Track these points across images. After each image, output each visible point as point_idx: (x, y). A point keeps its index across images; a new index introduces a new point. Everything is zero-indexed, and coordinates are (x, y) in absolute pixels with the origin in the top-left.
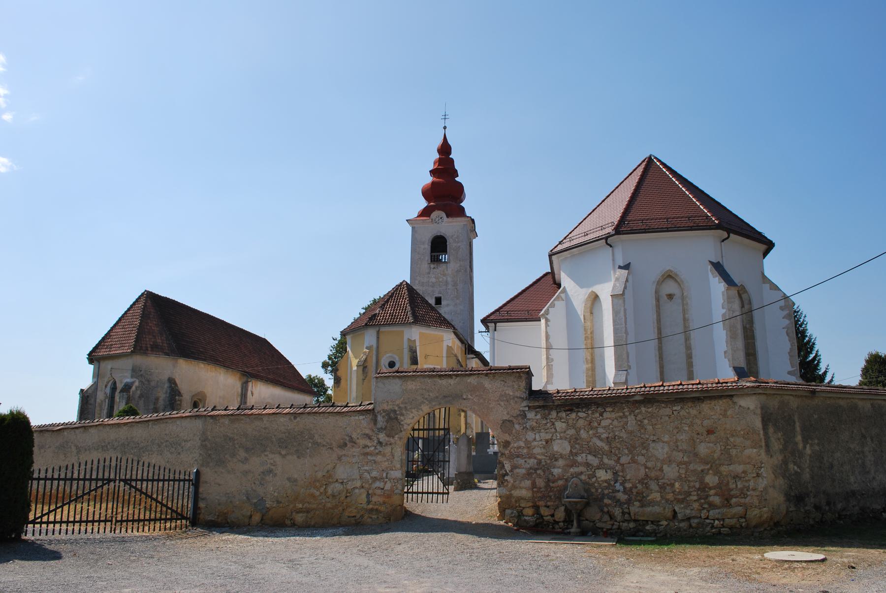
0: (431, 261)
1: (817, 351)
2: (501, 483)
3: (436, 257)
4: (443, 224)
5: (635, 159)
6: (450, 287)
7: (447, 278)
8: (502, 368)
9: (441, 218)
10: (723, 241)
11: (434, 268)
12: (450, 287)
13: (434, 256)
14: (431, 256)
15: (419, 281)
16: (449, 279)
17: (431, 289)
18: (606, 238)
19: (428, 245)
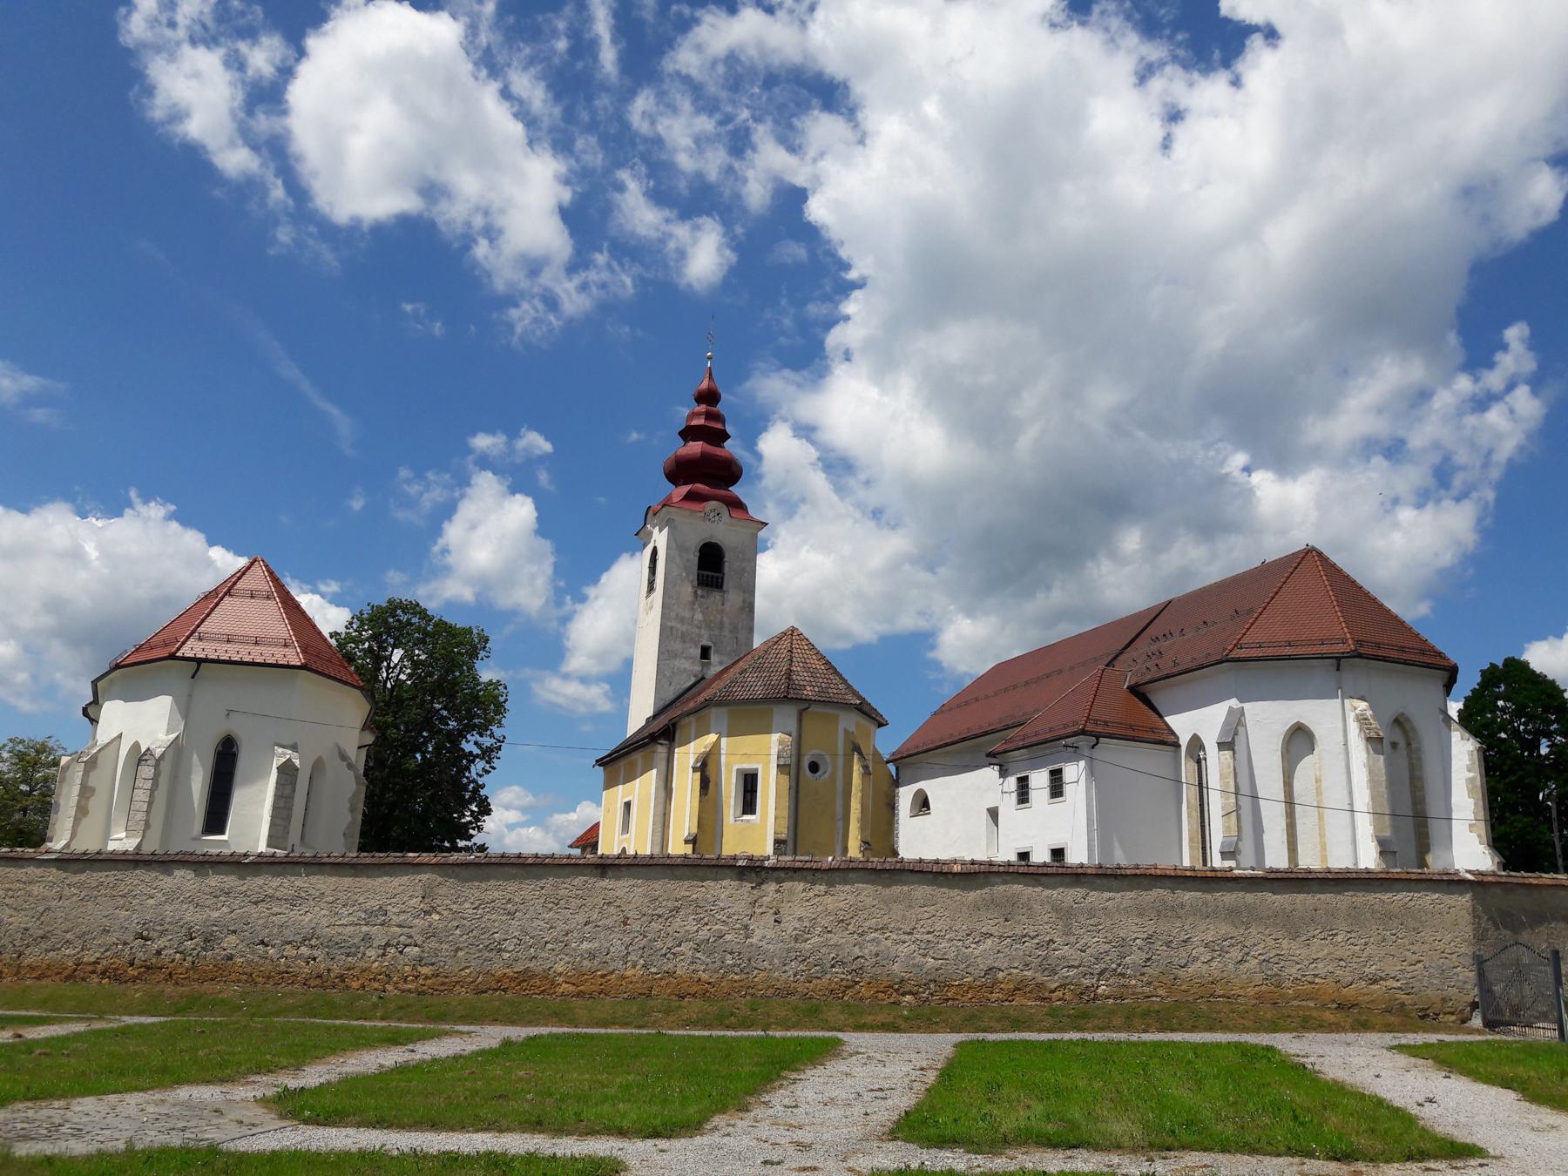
0: (698, 584)
1: (655, 541)
2: (595, 1021)
3: (715, 580)
4: (721, 524)
5: (985, 811)
6: (726, 633)
7: (722, 617)
8: (280, 869)
9: (718, 514)
10: (1093, 747)
11: (702, 597)
12: (726, 633)
13: (703, 575)
14: (698, 575)
15: (677, 615)
16: (726, 620)
17: (697, 631)
18: (1338, 659)
19: (695, 556)
